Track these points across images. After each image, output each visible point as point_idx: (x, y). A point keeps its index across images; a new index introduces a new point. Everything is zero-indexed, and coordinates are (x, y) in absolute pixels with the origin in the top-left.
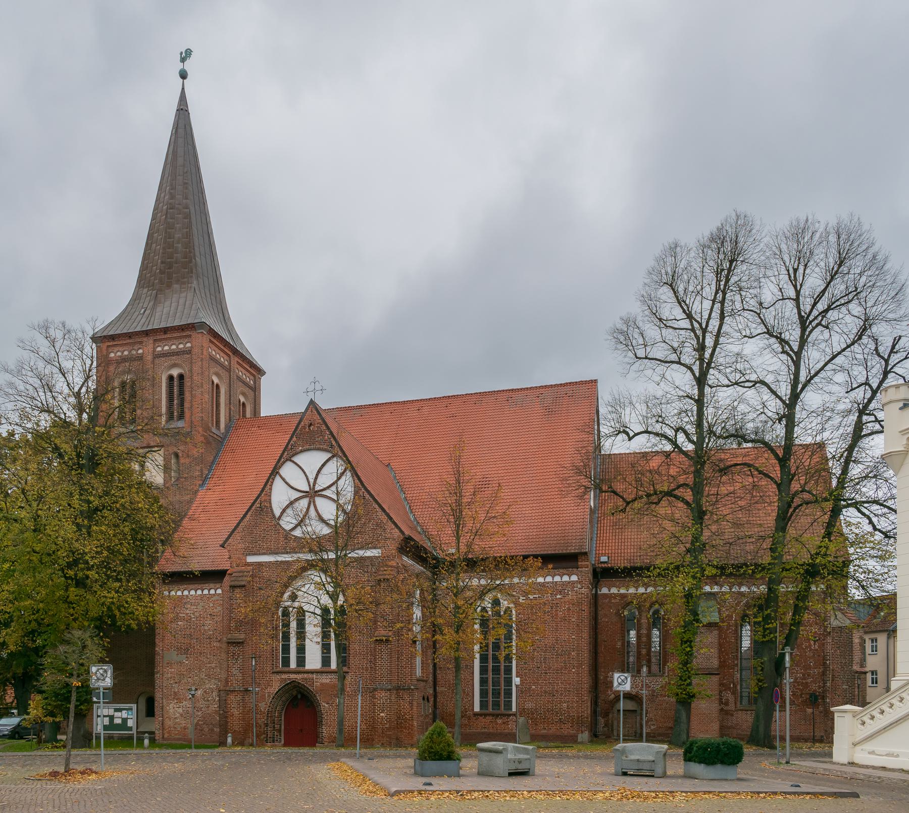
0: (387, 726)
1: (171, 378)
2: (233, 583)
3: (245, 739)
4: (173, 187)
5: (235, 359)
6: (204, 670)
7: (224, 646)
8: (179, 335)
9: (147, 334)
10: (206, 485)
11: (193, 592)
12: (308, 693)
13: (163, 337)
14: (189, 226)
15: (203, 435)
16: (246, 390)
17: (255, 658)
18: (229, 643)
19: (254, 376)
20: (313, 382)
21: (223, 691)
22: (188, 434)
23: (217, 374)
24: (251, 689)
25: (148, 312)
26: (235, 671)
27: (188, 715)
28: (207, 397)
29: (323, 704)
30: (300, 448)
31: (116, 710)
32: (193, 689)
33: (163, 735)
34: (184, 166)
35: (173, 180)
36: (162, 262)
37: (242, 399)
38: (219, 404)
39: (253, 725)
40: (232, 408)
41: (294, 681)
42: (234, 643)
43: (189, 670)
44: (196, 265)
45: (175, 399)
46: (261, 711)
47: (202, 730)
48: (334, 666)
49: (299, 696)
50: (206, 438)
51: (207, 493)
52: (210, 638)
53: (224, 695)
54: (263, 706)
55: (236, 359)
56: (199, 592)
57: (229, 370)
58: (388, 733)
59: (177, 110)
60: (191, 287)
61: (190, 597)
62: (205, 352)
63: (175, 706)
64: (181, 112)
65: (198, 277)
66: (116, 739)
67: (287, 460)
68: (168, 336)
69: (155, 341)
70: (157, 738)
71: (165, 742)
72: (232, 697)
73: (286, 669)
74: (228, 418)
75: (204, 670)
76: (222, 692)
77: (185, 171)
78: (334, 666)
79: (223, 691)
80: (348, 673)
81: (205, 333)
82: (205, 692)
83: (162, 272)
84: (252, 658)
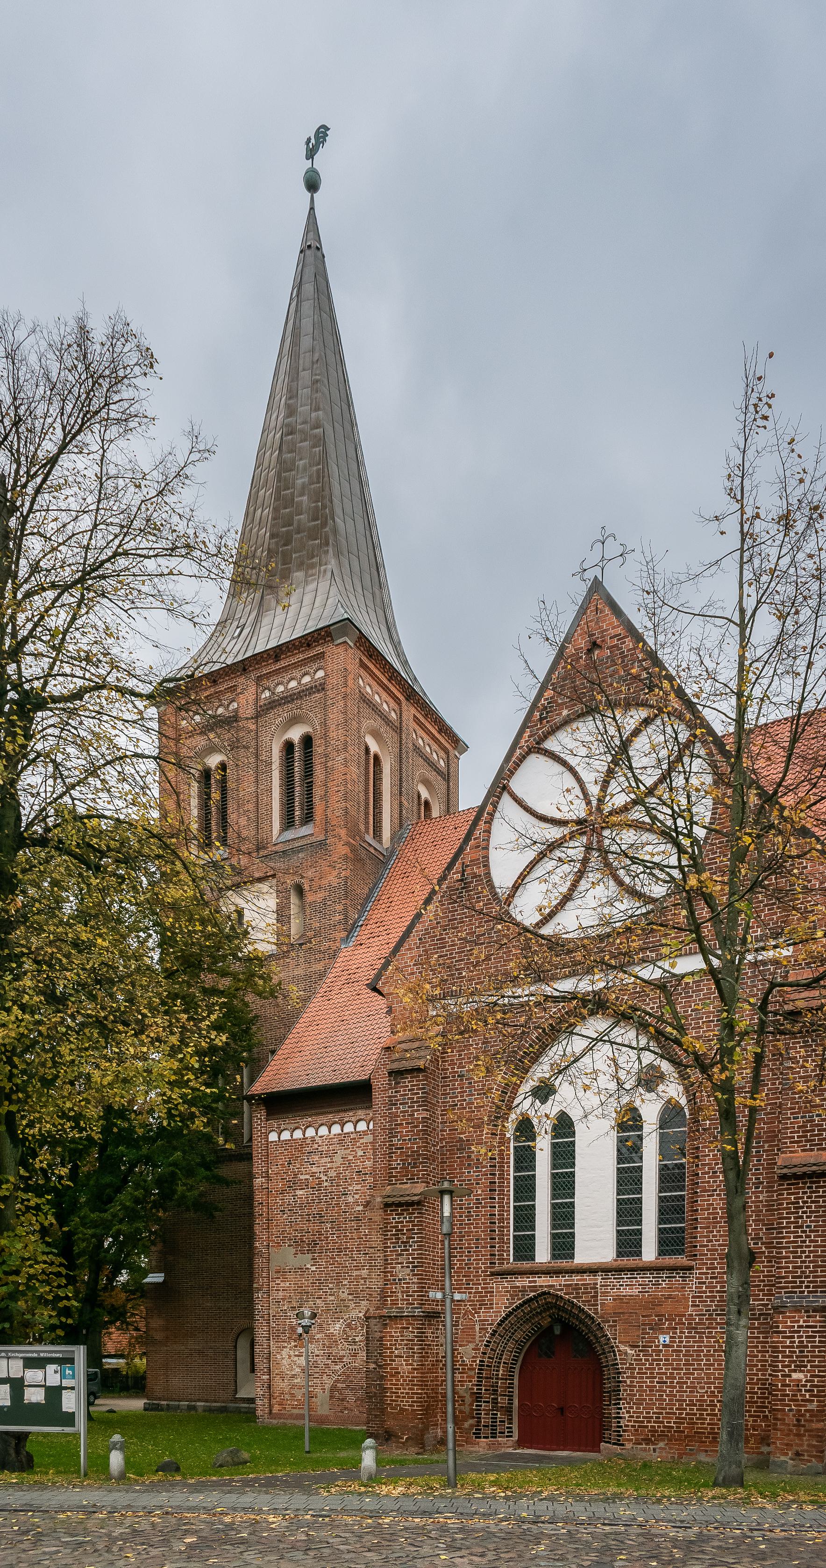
0: (813, 1406)
1: (289, 747)
2: (395, 1066)
3: (426, 1429)
4: (292, 394)
5: (410, 711)
6: (345, 1282)
7: (377, 1216)
8: (301, 657)
9: (244, 670)
10: (353, 939)
11: (323, 1131)
12: (582, 1322)
13: (273, 668)
14: (323, 459)
15: (347, 844)
16: (432, 776)
17: (450, 1192)
18: (387, 1205)
19: (447, 752)
20: (599, 541)
21: (375, 1318)
22: (322, 844)
23: (376, 735)
24: (439, 1295)
25: (246, 632)
26: (401, 1272)
27: (317, 1370)
28: (355, 771)
29: (622, 1347)
30: (565, 712)
31: (31, 1363)
32: (307, 1313)
33: (271, 1407)
34: (313, 350)
35: (292, 381)
36: (272, 536)
37: (425, 794)
38: (381, 794)
39: (444, 1396)
40: (405, 802)
41: (544, 1293)
42: (400, 1204)
43: (320, 1283)
44: (335, 531)
45: (297, 784)
46: (463, 1364)
47: (343, 1400)
48: (649, 1252)
49: (557, 1331)
50: (353, 850)
51: (356, 952)
52: (357, 1219)
53: (376, 1328)
54: (468, 1353)
55: (413, 711)
56: (336, 1129)
57: (398, 729)
58: (815, 1425)
59: (301, 252)
60: (325, 571)
61: (317, 1138)
62: (350, 682)
63: (292, 1353)
64: (308, 252)
65: (338, 554)
66: (200, 1410)
67: (529, 752)
68: (283, 663)
69: (259, 679)
70: (259, 1413)
71: (275, 1421)
72: (394, 1331)
73: (526, 1265)
74: (397, 821)
75: (345, 1282)
76: (373, 1322)
77: (315, 359)
78: (649, 1252)
79: (375, 1318)
80: (690, 1268)
81: (351, 644)
82: (349, 1325)
83: (271, 553)
84: (442, 1192)
